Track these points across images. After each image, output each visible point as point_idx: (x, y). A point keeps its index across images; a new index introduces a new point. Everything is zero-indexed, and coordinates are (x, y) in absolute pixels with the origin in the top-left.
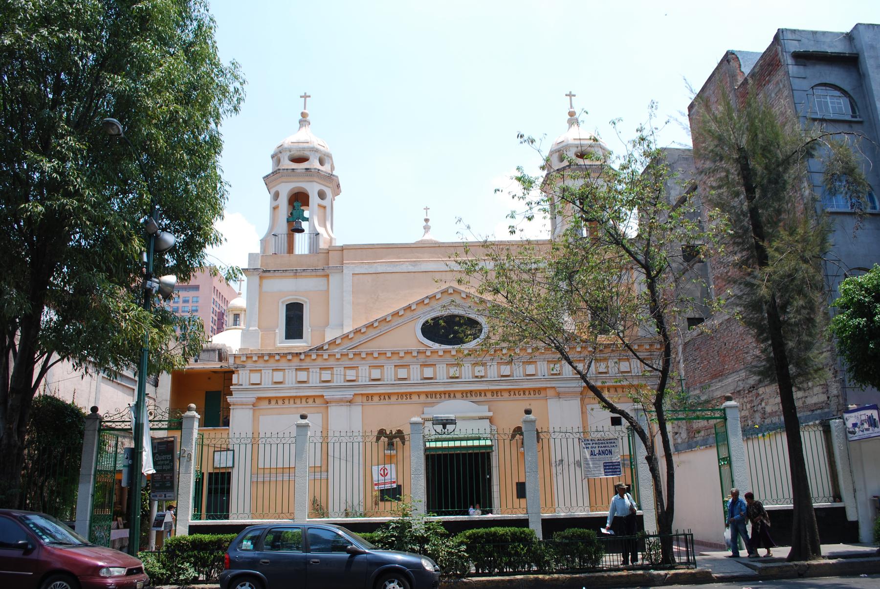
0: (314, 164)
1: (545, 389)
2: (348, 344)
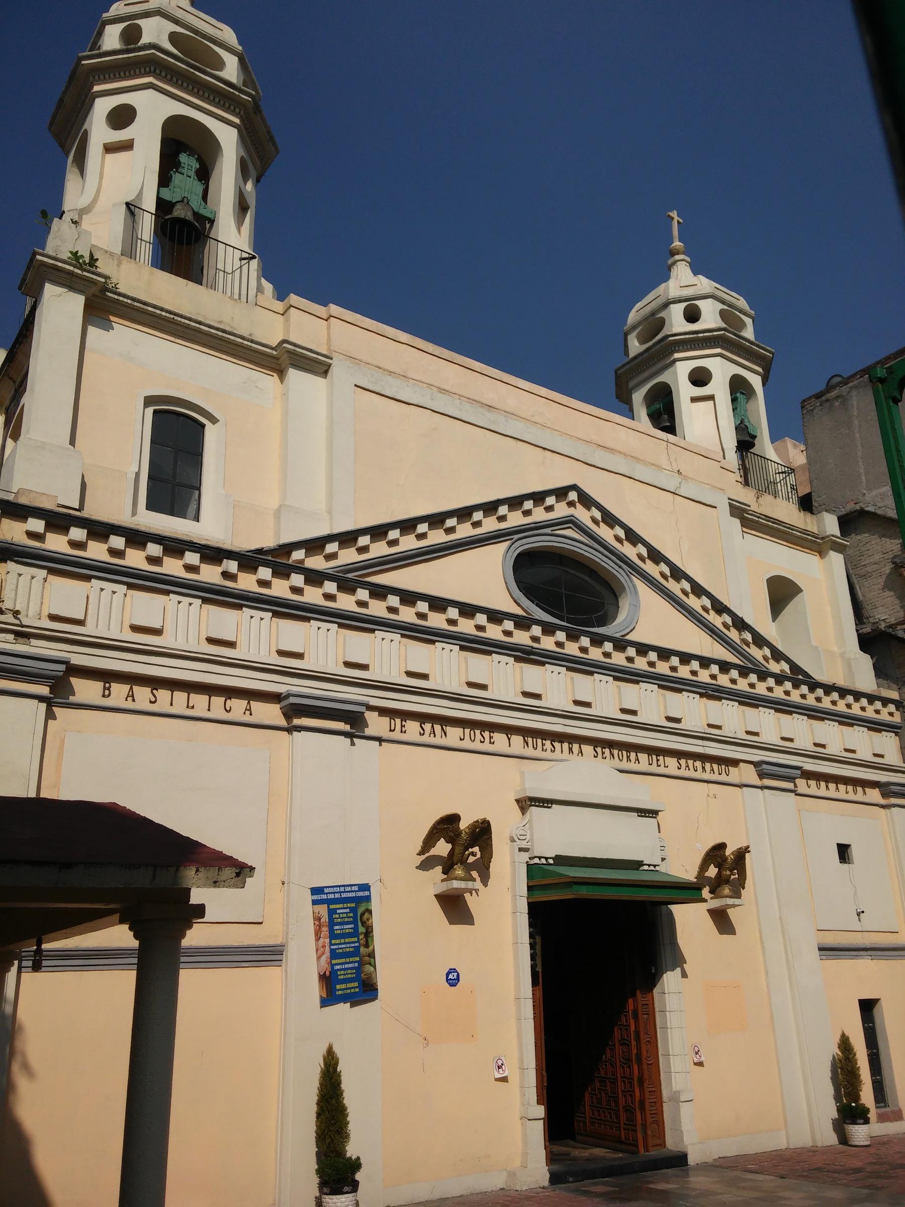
1: (735, 763)
2: (349, 556)
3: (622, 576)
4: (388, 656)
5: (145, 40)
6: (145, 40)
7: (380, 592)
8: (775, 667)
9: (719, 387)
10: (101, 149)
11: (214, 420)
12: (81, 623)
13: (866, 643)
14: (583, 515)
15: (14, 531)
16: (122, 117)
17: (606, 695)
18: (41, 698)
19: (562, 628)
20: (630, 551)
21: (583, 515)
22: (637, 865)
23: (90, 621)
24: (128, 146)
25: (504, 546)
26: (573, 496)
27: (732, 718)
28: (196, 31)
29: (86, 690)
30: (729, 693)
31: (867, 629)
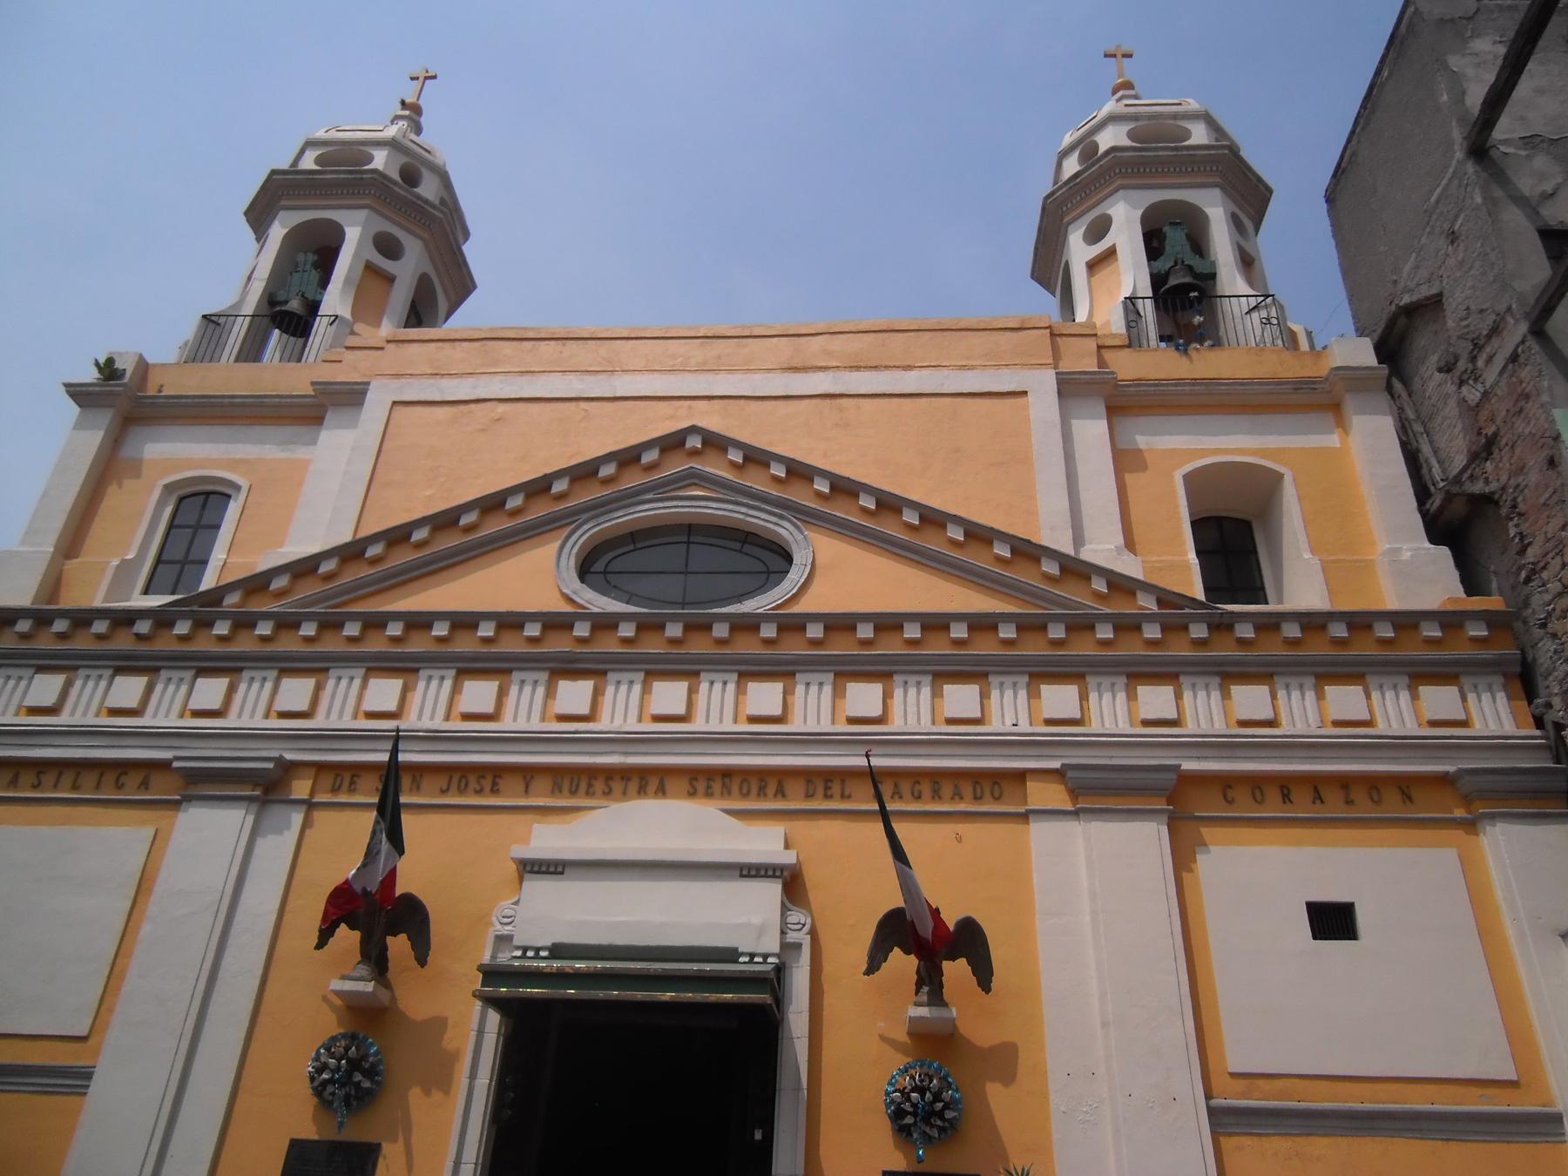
0: (428, 189)
1: (1021, 776)
3: (785, 531)
4: (431, 705)
5: (1102, 149)
6: (1102, 149)
7: (375, 623)
8: (1122, 607)
9: (1126, 234)
10: (1084, 269)
11: (238, 488)
12: (1464, 724)
13: (1440, 529)
14: (713, 467)
15: (7, 641)
16: (1099, 230)
17: (718, 706)
18: (250, 799)
19: (674, 618)
20: (798, 495)
21: (713, 467)
22: (731, 955)
23: (1284, 718)
24: (1111, 253)
25: (797, 609)
26: (694, 442)
27: (1010, 710)
28: (1151, 117)
29: (301, 788)
30: (1288, 664)
31: (1435, 503)
